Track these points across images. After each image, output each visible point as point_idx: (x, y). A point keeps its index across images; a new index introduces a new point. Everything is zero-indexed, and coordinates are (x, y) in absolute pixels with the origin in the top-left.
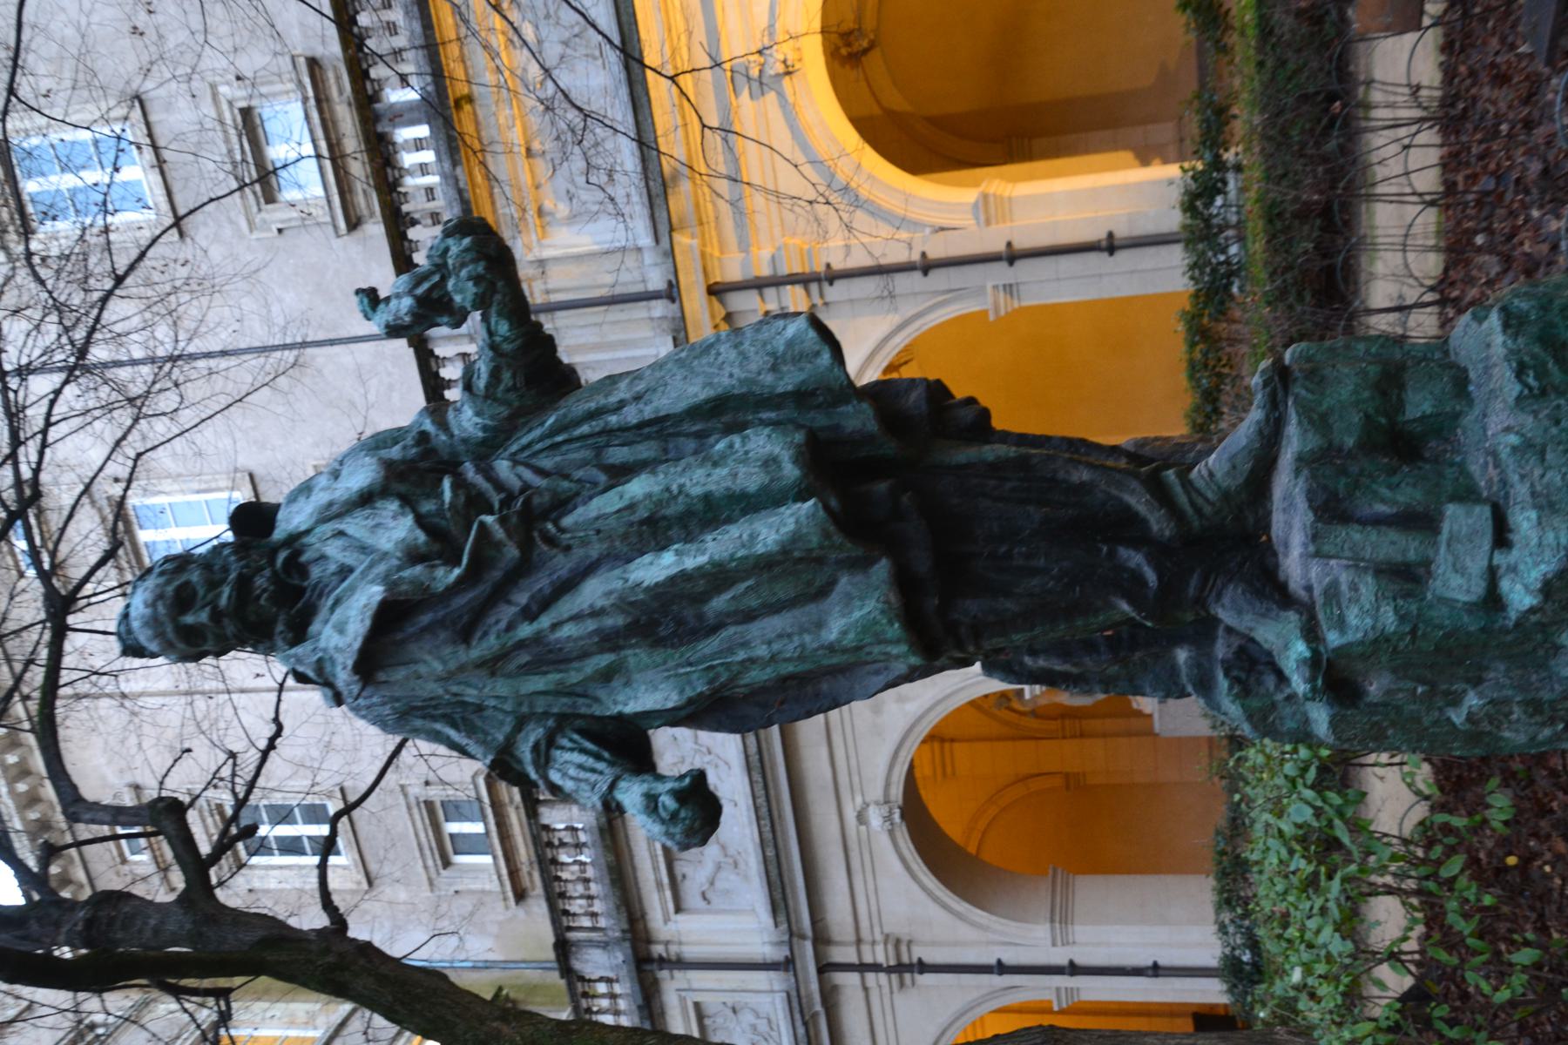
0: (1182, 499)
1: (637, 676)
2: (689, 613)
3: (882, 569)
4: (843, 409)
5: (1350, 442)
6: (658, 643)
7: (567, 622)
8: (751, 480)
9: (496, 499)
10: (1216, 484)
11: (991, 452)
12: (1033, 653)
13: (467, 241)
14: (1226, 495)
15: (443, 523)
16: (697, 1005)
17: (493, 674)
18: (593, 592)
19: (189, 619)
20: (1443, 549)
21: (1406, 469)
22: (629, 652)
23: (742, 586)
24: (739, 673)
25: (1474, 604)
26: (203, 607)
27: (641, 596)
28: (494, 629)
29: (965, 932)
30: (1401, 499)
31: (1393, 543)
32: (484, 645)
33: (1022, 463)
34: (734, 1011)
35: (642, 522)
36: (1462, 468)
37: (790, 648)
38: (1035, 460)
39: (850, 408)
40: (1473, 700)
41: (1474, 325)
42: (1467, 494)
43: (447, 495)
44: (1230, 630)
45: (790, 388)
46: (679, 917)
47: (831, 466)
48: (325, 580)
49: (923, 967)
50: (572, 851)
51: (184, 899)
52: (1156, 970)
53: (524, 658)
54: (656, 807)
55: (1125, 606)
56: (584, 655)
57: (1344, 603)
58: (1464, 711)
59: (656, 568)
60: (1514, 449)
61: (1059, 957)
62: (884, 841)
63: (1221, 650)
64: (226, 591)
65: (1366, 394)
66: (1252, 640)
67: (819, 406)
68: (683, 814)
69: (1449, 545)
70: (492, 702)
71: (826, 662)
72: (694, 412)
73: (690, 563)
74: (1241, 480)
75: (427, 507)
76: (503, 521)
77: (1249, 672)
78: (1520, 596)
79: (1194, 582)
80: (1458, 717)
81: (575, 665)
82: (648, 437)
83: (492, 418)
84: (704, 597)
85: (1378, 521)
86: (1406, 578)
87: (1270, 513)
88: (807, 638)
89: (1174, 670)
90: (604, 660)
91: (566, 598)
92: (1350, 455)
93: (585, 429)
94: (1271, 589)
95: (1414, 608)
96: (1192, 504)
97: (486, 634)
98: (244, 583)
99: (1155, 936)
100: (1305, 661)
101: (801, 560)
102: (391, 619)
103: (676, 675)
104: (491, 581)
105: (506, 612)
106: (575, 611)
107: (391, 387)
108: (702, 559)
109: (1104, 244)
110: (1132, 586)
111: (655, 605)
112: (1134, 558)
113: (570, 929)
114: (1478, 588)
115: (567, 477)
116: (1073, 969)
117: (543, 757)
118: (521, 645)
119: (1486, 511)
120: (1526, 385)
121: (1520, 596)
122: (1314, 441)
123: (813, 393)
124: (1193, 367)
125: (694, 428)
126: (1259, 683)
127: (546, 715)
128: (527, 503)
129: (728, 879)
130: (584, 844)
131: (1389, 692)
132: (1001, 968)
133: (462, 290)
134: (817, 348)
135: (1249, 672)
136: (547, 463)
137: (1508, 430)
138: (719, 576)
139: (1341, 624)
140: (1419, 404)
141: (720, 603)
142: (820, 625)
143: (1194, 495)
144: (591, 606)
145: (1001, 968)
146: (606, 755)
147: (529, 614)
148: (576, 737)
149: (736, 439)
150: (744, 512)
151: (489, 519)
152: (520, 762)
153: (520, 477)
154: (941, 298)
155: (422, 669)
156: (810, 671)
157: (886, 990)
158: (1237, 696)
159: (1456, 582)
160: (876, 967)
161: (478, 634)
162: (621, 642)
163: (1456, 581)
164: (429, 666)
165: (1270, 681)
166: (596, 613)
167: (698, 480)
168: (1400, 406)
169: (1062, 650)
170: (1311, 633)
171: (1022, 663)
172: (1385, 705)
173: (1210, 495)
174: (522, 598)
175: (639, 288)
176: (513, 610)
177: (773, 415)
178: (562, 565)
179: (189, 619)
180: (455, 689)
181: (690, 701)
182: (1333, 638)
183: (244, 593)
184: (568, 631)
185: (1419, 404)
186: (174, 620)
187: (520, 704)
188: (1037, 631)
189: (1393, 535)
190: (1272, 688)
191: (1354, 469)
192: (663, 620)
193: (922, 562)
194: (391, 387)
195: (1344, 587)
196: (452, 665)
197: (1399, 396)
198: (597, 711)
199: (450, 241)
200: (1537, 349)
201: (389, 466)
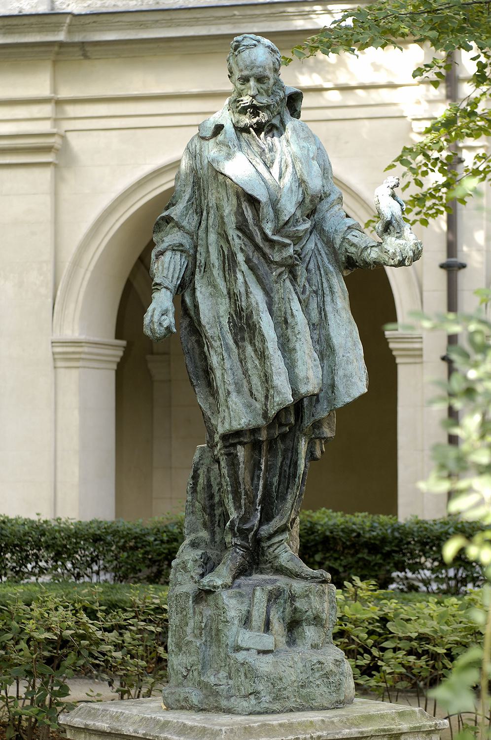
0: (276, 539)
7: (243, 277)
23: (257, 362)
32: (235, 237)
59: (267, 324)
68: (161, 328)
69: (259, 635)
72: (328, 339)
91: (255, 279)
93: (325, 285)
96: (274, 544)
104: (261, 249)
105: (250, 250)
106: (250, 285)
114: (244, 645)
124: (434, 521)
134: (352, 395)
138: (262, 356)
143: (278, 545)
144: (251, 293)
147: (248, 261)
161: (240, 235)
170: (226, 587)
176: (251, 254)
188: (228, 479)
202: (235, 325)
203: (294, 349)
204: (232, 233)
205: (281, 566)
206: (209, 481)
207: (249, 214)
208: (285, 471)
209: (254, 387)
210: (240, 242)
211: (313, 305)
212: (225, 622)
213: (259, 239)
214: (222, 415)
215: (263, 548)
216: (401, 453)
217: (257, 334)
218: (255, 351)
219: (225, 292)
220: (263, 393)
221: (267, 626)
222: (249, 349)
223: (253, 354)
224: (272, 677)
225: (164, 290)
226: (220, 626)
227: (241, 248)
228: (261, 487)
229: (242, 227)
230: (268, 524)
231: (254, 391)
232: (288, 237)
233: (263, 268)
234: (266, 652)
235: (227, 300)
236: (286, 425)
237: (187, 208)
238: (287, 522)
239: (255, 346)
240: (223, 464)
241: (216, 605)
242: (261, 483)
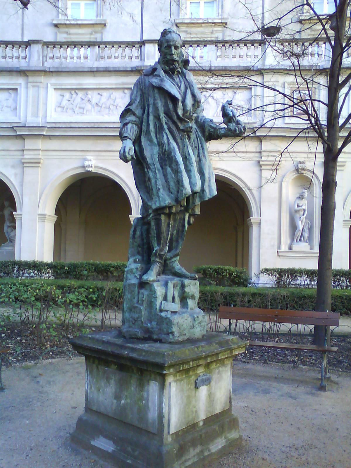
7: (167, 136)
18: (174, 144)
32: (163, 117)
84: (171, 166)
99: (35, 239)
107: (126, 25)
133: (232, 126)
138: (177, 172)
144: (171, 143)
147: (169, 129)
154: (19, 194)
184: (165, 135)
194: (126, 25)
202: (161, 159)
204: (162, 115)
205: (176, 272)
206: (142, 233)
207: (171, 106)
209: (171, 187)
210: (165, 119)
213: (175, 118)
214: (154, 200)
218: (172, 170)
219: (156, 143)
220: (176, 189)
221: (173, 300)
222: (169, 170)
223: (171, 172)
225: (128, 140)
226: (153, 300)
227: (166, 122)
228: (169, 235)
229: (167, 113)
231: (171, 189)
233: (176, 133)
235: (158, 147)
239: (172, 167)
241: (151, 290)
242: (170, 233)
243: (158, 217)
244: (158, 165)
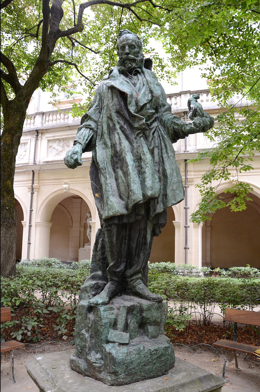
0: (134, 278)
1: (105, 151)
2: (119, 165)
3: (124, 212)
4: (162, 205)
5: (144, 315)
6: (112, 157)
7: (119, 137)
8: (149, 183)
9: (149, 122)
10: (137, 285)
11: (149, 236)
12: (103, 240)
13: (209, 123)
14: (135, 287)
15: (144, 110)
16: (27, 143)
17: (108, 117)
18: (125, 143)
19: (127, 47)
20: (120, 333)
21: (137, 325)
22: (110, 150)
23: (124, 179)
24: (104, 175)
25: (107, 338)
26: (129, 51)
27: (123, 155)
28: (118, 119)
29: (40, 203)
30: (131, 324)
31: (122, 323)
32: (115, 116)
33: (145, 244)
34: (25, 151)
35: (140, 156)
36: (135, 336)
37: (108, 188)
38: (146, 246)
39: (162, 206)
40: (87, 335)
41: (166, 340)
42: (131, 338)
43: (150, 111)
44: (105, 285)
45: (168, 193)
46: (47, 140)
47: (149, 202)
48: (133, 80)
49: (32, 194)
50: (63, 117)
51: (59, 31)
52: (29, 244)
53: (111, 125)
54: (74, 154)
55: (112, 264)
56: (111, 139)
57: (109, 311)
58: (85, 333)
59: (129, 158)
60: (140, 348)
61: (33, 224)
62: (60, 188)
63: (100, 282)
64: (133, 57)
65: (154, 318)
66: (102, 290)
67: (163, 199)
70: (101, 116)
71: (105, 196)
72: (164, 170)
73: (130, 168)
74: (138, 290)
75: (148, 106)
76: (144, 124)
77: (95, 288)
78: (108, 348)
79: (116, 279)
80: (83, 331)
81: (108, 137)
82: (160, 159)
83: (167, 122)
84: (122, 169)
85: (127, 320)
86: (114, 325)
87: (130, 295)
88: (111, 193)
89: (96, 271)
90: (109, 144)
91: (124, 137)
92: (141, 315)
93: (163, 144)
94: (113, 295)
95: (107, 326)
96: (133, 279)
97: (118, 117)
98: (134, 60)
100: (97, 302)
101: (129, 193)
102: (123, 95)
103: (104, 160)
104: (129, 120)
105: (122, 123)
106: (121, 139)
108: (131, 171)
109: (187, 247)
110: (116, 265)
111: (121, 158)
112: (122, 267)
113: (46, 115)
114: (111, 340)
115: (152, 139)
116: (30, 226)
117: (87, 127)
118: (114, 125)
119: (127, 342)
120: (153, 351)
121: (108, 348)
122: (145, 307)
123: (166, 198)
125: (160, 170)
126: (93, 290)
127: (98, 128)
128: (147, 130)
129: (54, 152)
130: (64, 120)
131: (89, 319)
132: (31, 211)
135: (95, 288)
136: (156, 134)
137: (144, 347)
138: (126, 174)
139: (105, 311)
140: (151, 329)
141: (120, 173)
142: (113, 195)
145: (31, 211)
146: (87, 142)
147: (121, 128)
148: (92, 135)
149: (158, 180)
150: (141, 181)
151: (144, 121)
152: (87, 121)
153: (153, 128)
154: (178, 208)
155: (110, 101)
156: (103, 192)
157: (28, 185)
158: (90, 285)
159: (113, 335)
160: (33, 183)
162: (113, 149)
163: (113, 335)
164: (112, 103)
165: (93, 293)
166: (120, 143)
167: (148, 171)
168: (150, 325)
169: (103, 247)
170: (104, 304)
171: (100, 238)
172: (87, 317)
173: (135, 284)
174: (125, 127)
175: (188, 144)
177: (162, 188)
178: (132, 137)
179: (127, 47)
180: (105, 108)
181: (98, 163)
182: (102, 308)
183: (132, 62)
184: (117, 136)
185: (151, 329)
186: (127, 44)
187: (100, 122)
189: (124, 323)
190: (92, 293)
191: (138, 315)
192: (117, 159)
193: (125, 220)
195: (112, 311)
196: (111, 108)
197: (153, 325)
198: (97, 141)
199: (209, 119)
200: (160, 353)
201: (158, 98)
203: (145, 172)
208: (140, 241)
211: (156, 151)
212: (101, 325)
215: (128, 281)
216: (176, 246)
217: (124, 163)
224: (126, 362)
225: (78, 144)
230: (130, 269)
232: (143, 116)
234: (123, 344)
236: (140, 215)
237: (95, 110)
238: (141, 268)
240: (106, 236)
243: (109, 228)
244: (110, 169)
